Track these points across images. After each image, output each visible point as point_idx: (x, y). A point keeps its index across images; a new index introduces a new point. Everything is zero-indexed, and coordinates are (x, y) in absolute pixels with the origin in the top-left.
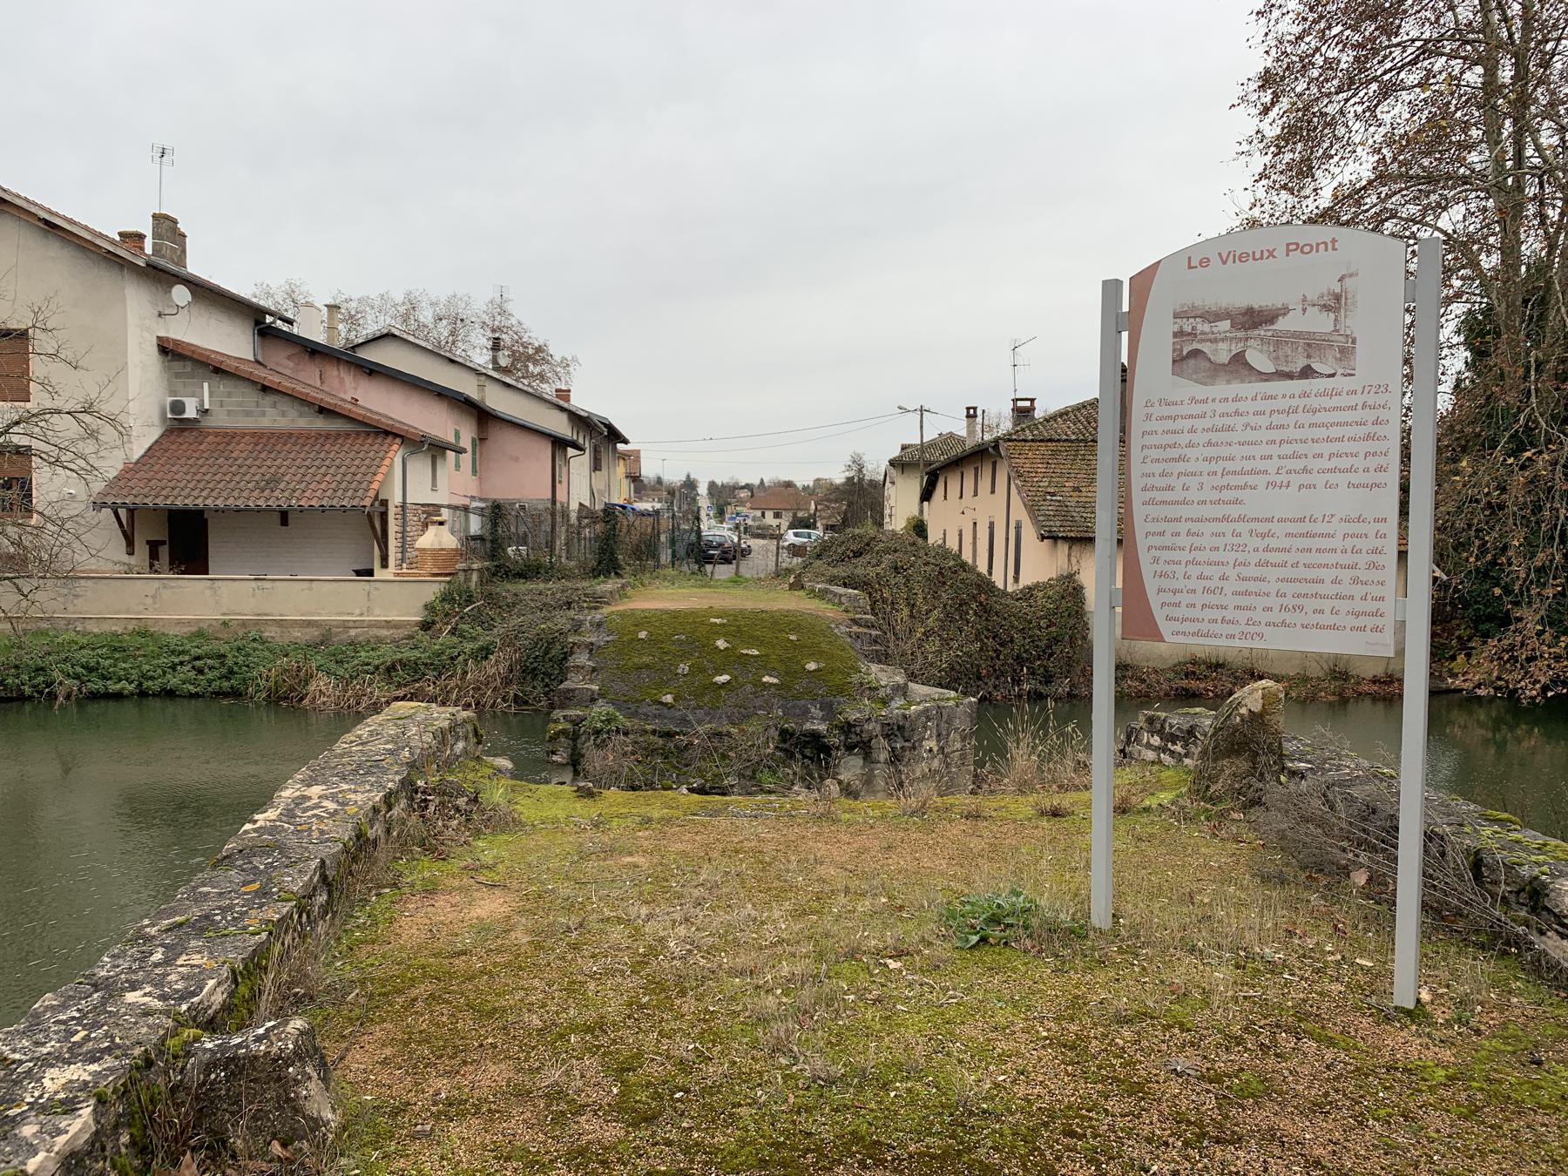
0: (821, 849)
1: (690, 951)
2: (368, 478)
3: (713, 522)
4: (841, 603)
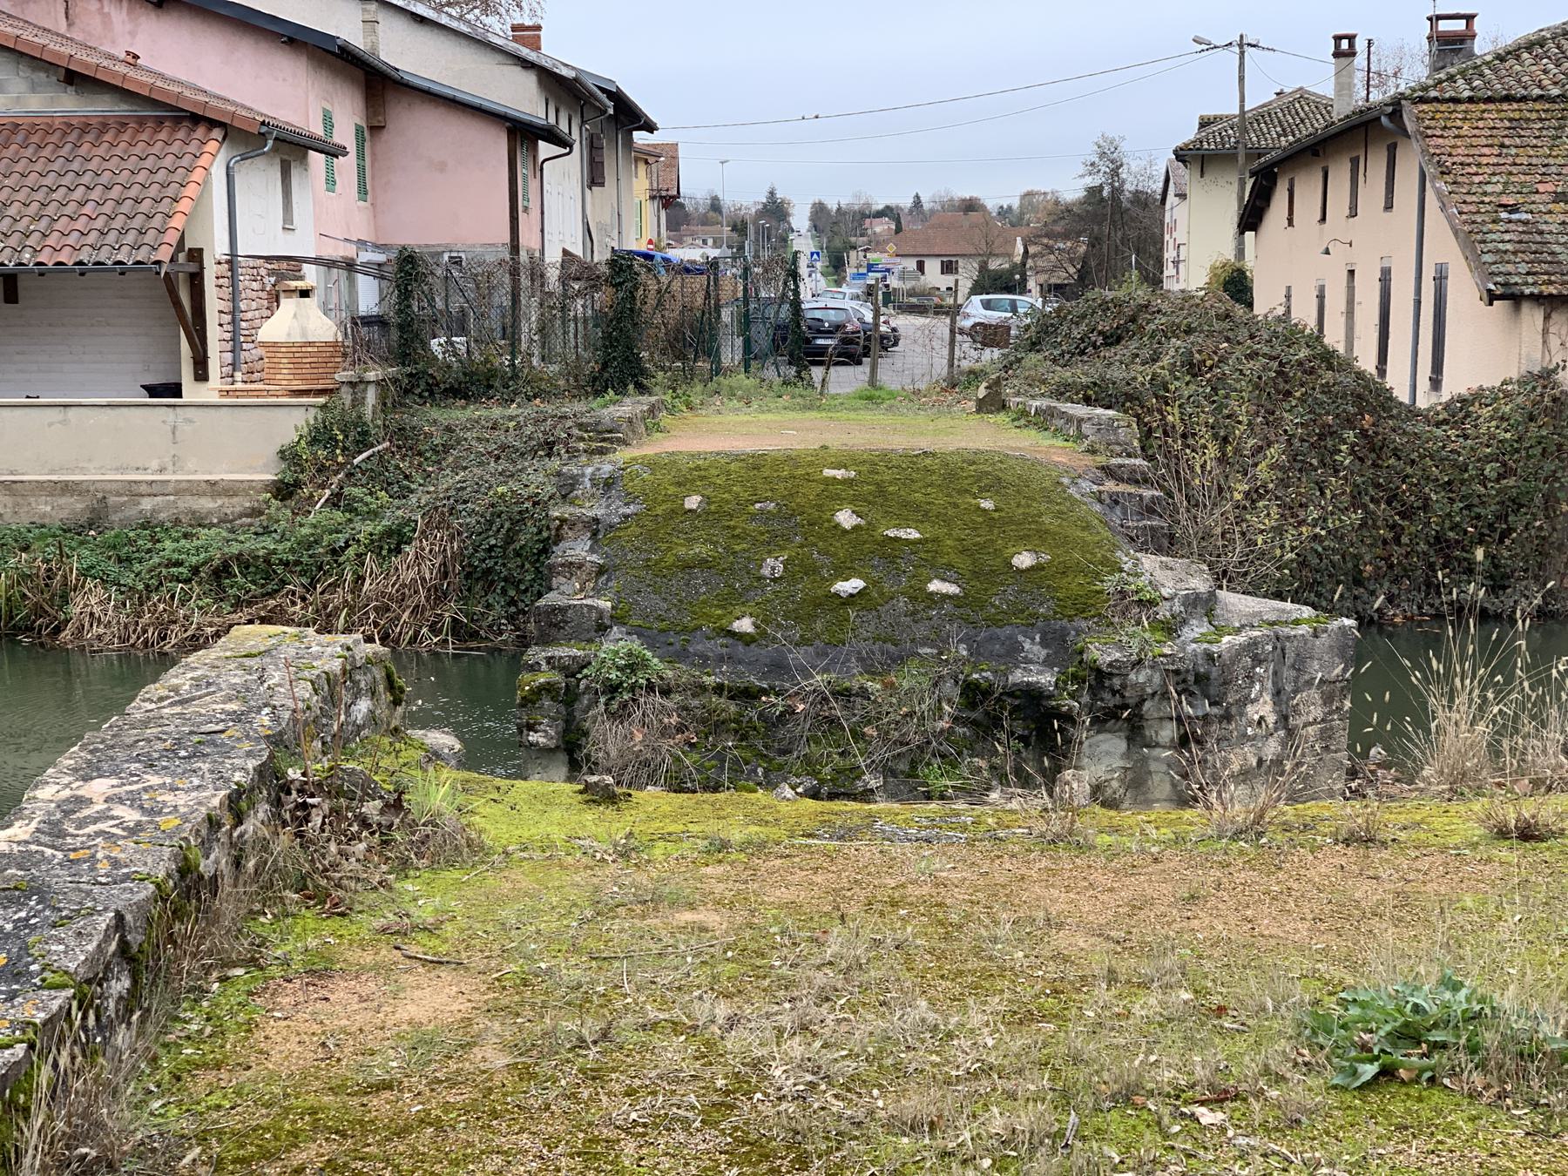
0: (1058, 900)
1: (812, 1086)
2: (164, 206)
3: (822, 283)
4: (1081, 436)
